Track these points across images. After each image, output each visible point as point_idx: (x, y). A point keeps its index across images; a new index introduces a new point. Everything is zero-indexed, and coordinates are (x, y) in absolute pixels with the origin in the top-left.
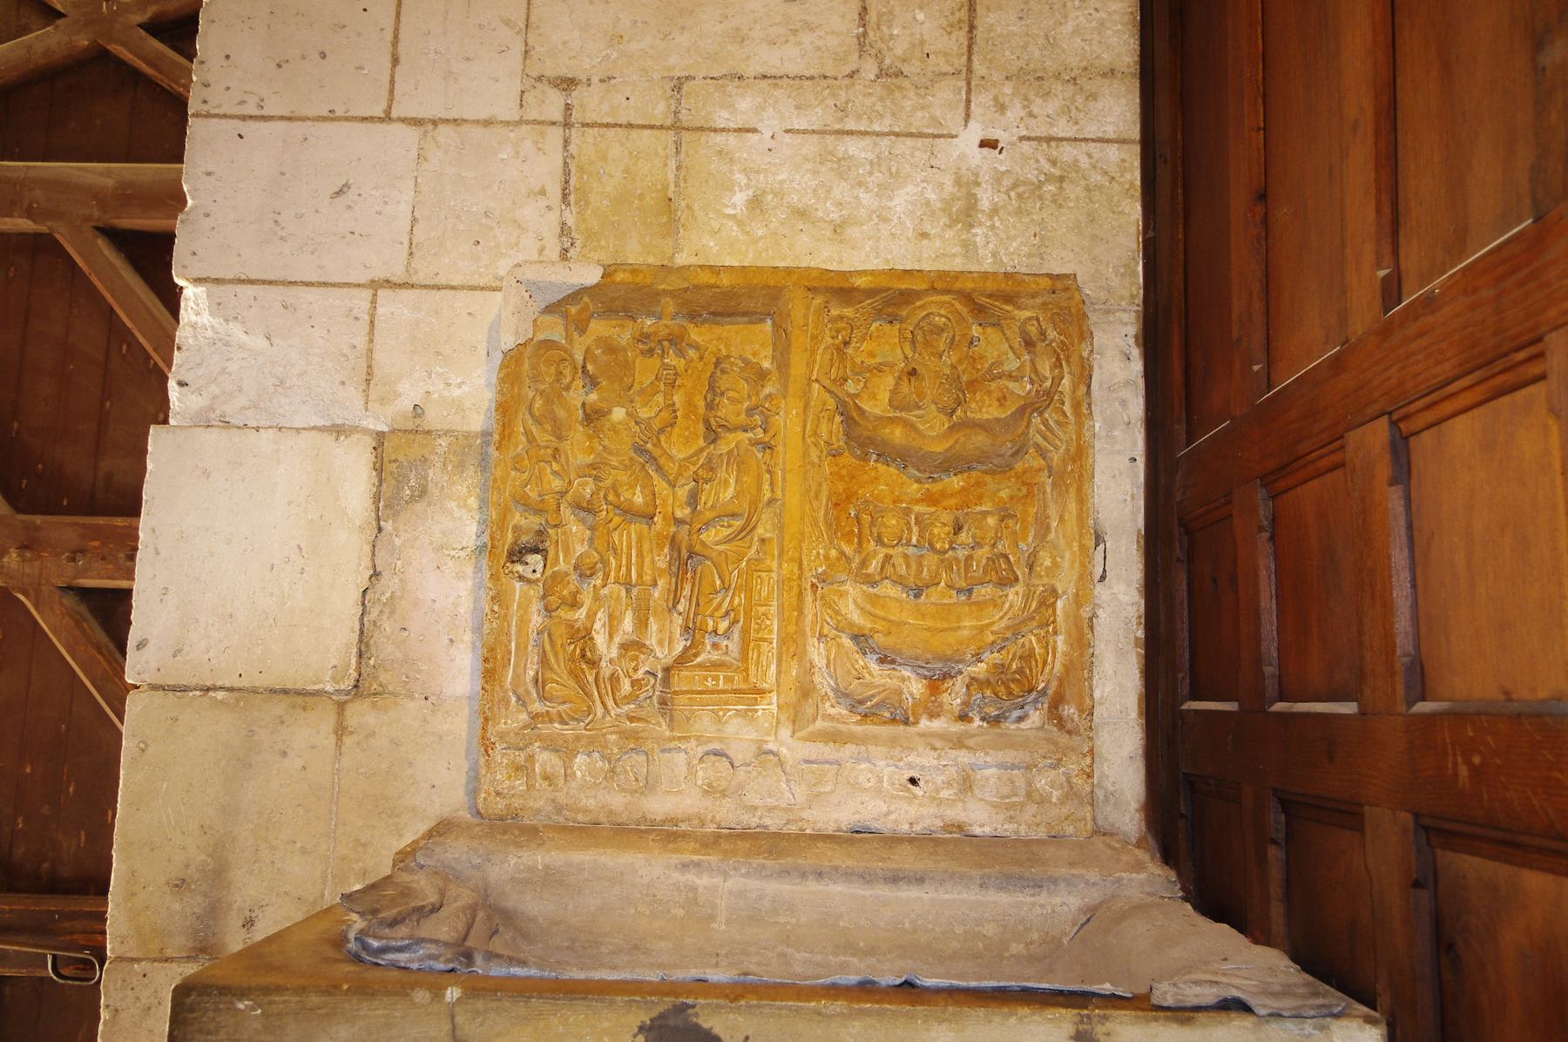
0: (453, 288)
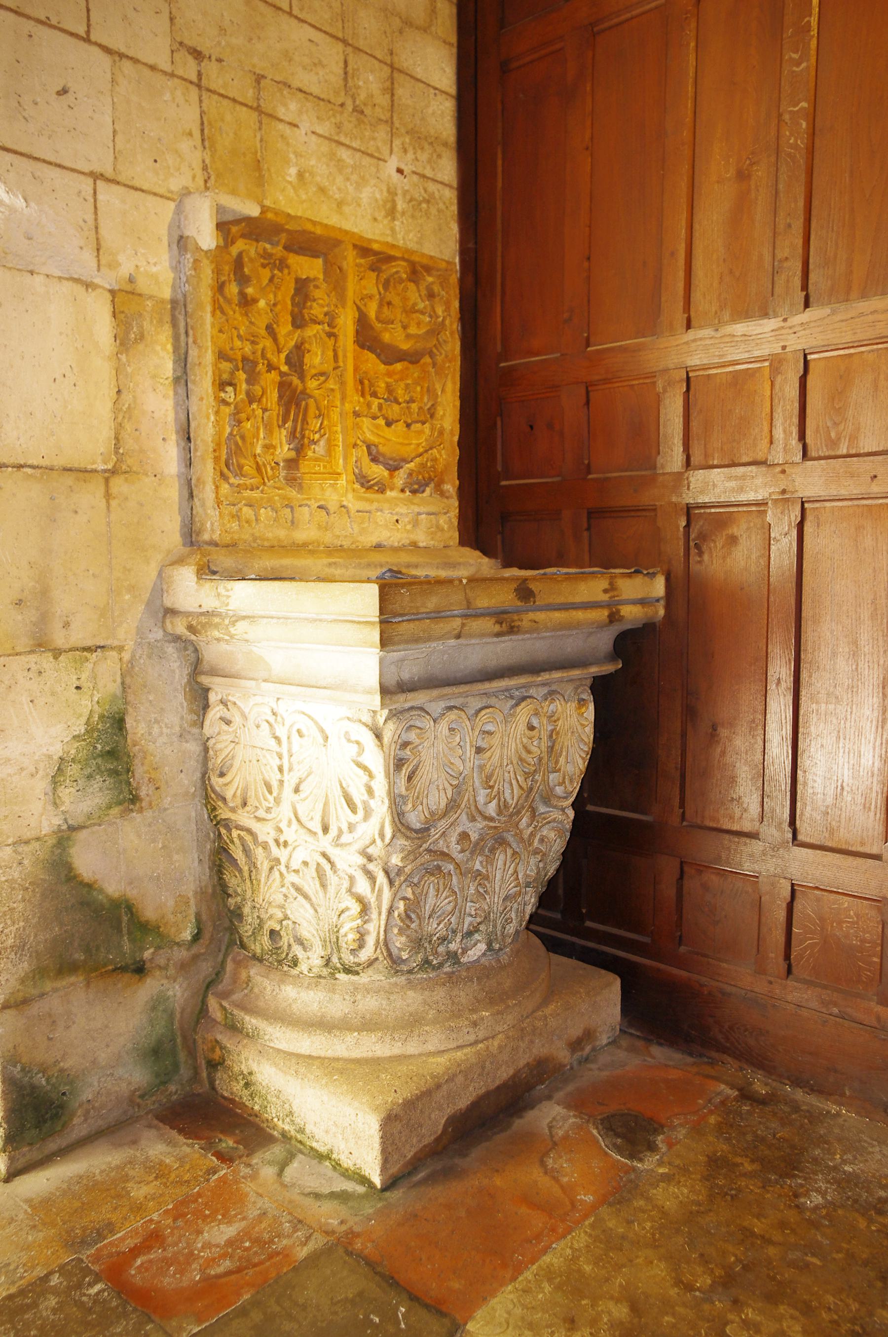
0: (143, 191)
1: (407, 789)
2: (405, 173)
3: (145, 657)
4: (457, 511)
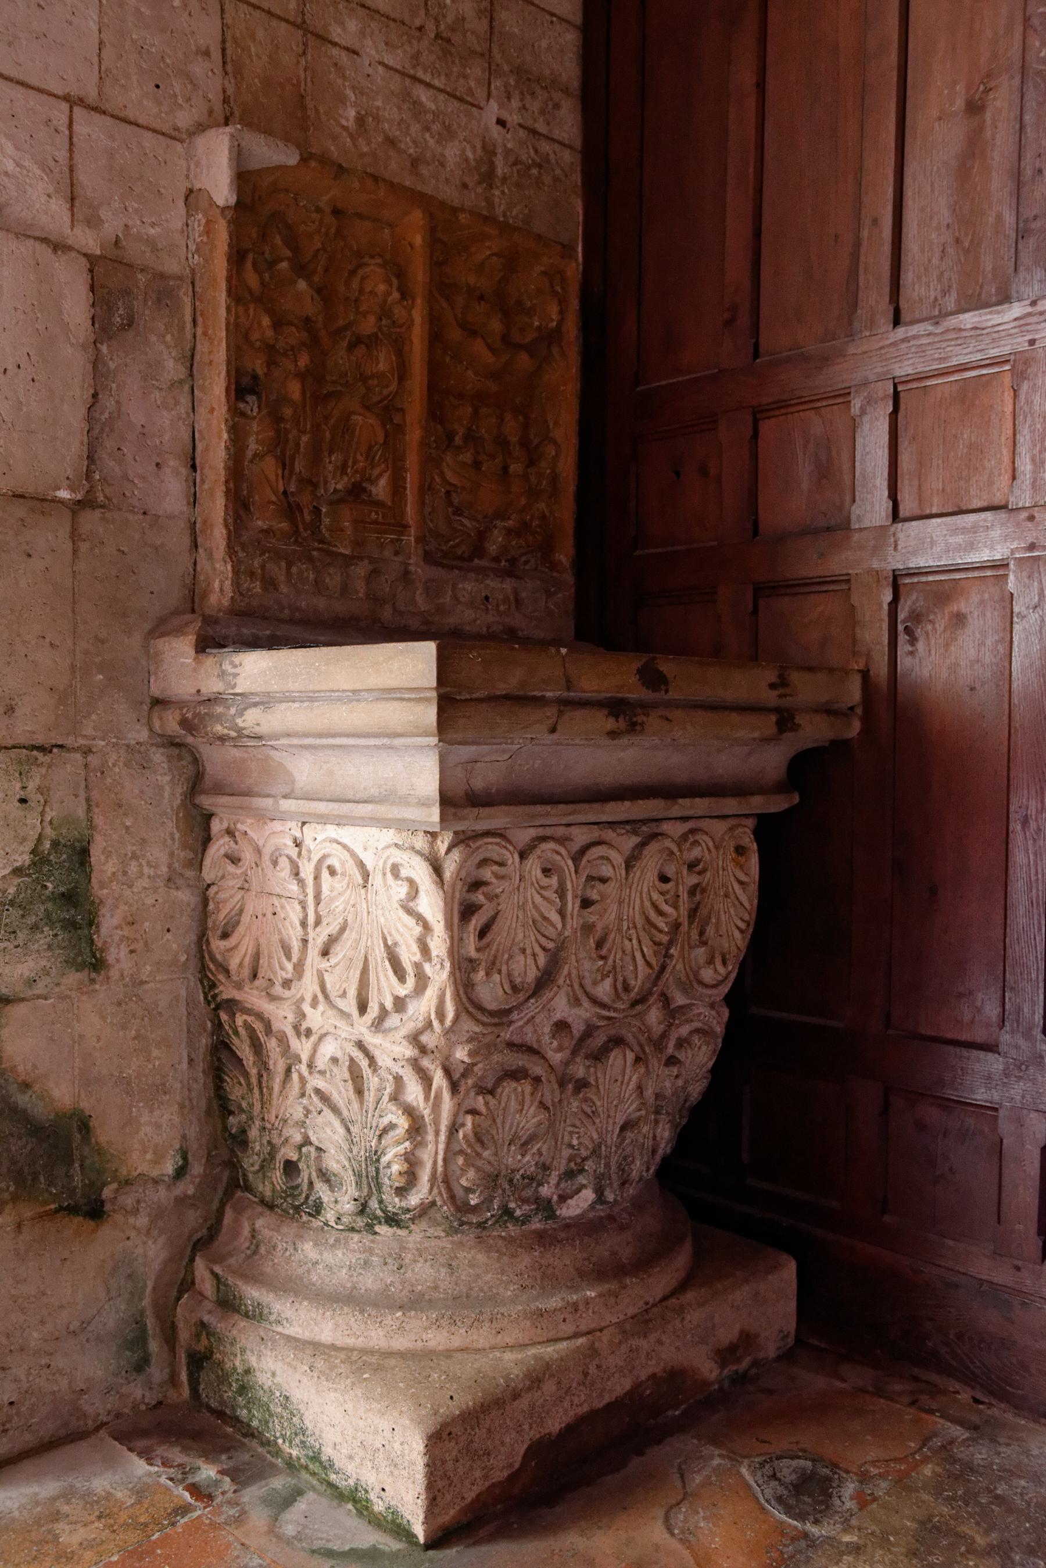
0: (138, 125)
1: (478, 950)
2: (508, 126)
3: (121, 764)
4: (573, 590)
